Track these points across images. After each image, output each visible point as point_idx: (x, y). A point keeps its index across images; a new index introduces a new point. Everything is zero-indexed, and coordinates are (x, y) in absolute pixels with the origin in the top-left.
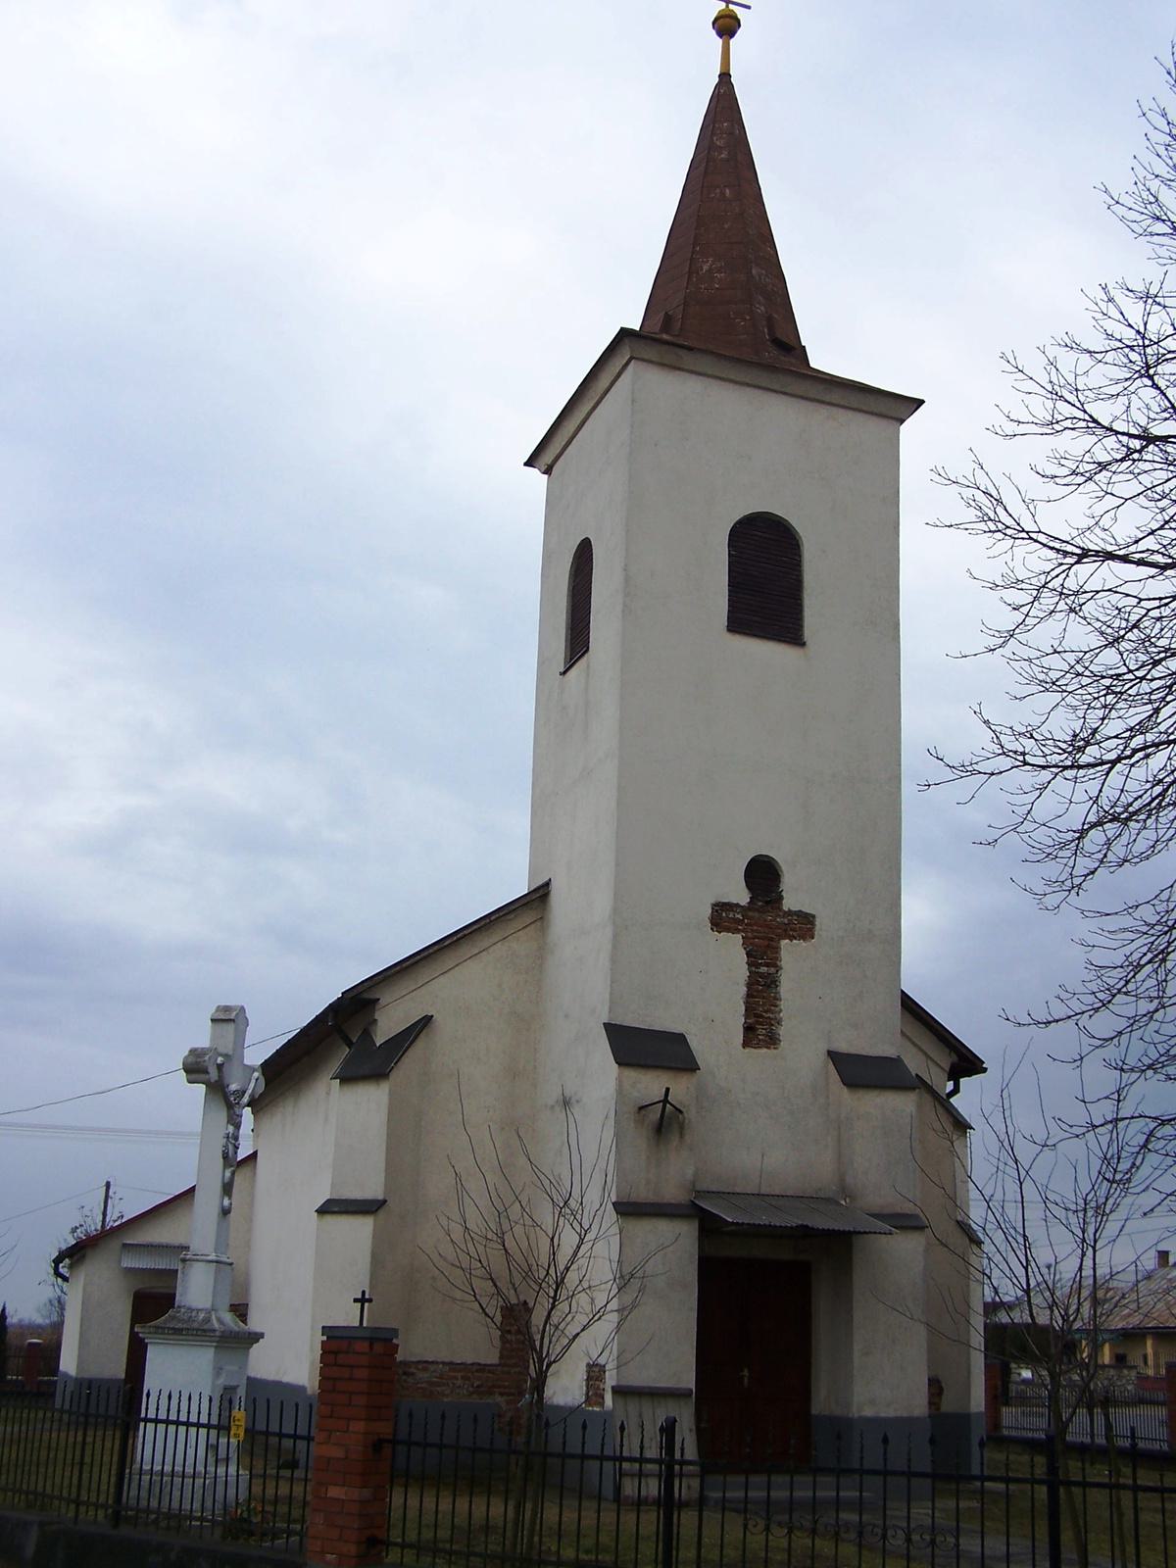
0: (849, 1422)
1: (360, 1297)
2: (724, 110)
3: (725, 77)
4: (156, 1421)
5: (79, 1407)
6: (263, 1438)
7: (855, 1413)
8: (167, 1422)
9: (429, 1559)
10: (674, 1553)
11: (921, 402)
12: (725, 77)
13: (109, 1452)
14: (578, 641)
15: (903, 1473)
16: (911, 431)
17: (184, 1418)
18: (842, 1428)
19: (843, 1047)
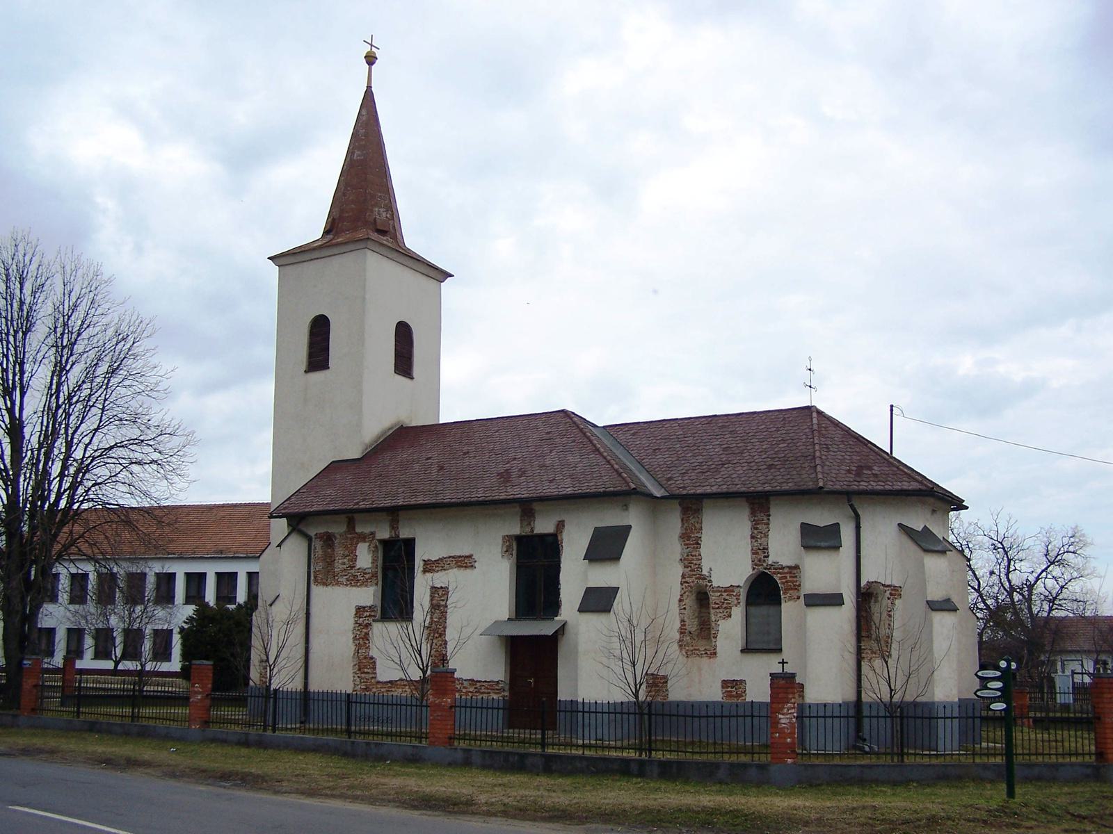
0: (933, 703)
1: (781, 661)
2: (369, 100)
3: (369, 88)
4: (461, 707)
5: (255, 701)
6: (581, 714)
7: (936, 699)
8: (493, 708)
9: (1061, 733)
10: (1014, 734)
11: (451, 276)
12: (369, 88)
13: (469, 726)
14: (404, 334)
15: (835, 717)
16: (446, 285)
17: (463, 709)
18: (574, 707)
19: (583, 558)
